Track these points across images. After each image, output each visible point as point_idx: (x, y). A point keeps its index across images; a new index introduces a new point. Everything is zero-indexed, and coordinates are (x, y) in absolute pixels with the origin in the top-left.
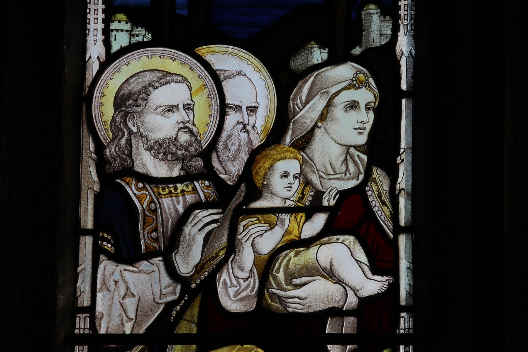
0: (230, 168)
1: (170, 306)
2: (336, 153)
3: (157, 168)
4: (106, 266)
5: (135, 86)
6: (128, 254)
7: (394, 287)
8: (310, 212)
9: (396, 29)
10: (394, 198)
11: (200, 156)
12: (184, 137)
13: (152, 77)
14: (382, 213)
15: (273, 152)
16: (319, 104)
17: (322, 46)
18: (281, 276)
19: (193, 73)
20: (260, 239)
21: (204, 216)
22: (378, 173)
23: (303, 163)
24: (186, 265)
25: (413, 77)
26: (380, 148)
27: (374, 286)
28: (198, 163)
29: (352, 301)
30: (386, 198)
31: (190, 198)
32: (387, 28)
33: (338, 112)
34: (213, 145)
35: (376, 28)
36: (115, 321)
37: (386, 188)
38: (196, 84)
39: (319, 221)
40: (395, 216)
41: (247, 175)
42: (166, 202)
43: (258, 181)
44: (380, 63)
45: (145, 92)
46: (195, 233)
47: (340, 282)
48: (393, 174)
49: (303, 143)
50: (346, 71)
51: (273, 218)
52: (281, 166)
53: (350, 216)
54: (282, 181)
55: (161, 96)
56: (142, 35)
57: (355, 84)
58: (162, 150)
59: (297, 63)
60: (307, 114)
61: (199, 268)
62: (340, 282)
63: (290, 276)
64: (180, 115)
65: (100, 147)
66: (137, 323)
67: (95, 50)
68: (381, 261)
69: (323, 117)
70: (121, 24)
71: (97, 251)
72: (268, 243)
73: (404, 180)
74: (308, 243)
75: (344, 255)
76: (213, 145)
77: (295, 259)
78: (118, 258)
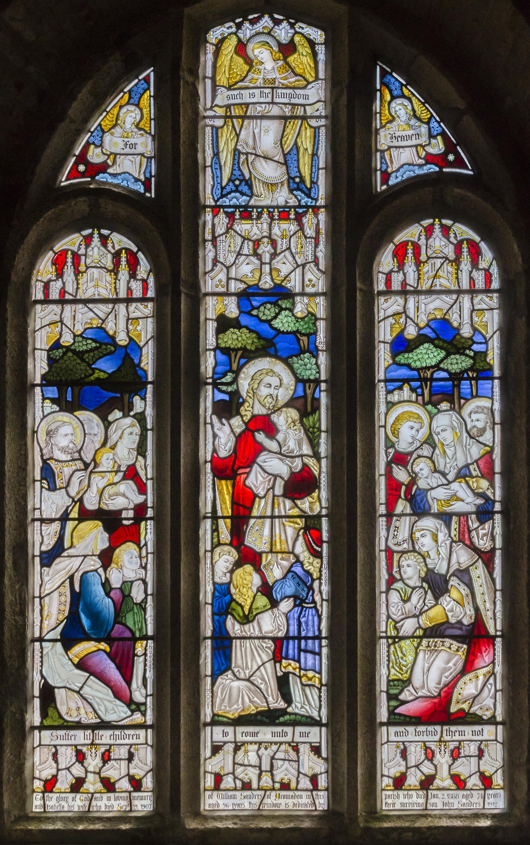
0: (88, 457)
1: (68, 507)
2: (126, 452)
3: (63, 457)
4: (45, 492)
5: (53, 427)
6: (52, 488)
7: (146, 500)
8: (117, 472)
9: (146, 405)
10: (147, 469)
11: (246, 52)
12: (71, 445)
13: (59, 423)
14: (142, 473)
15: (103, 450)
16: (119, 432)
17: (120, 410)
18: (107, 496)
19: (75, 422)
20: (98, 482)
21: (78, 474)
22: (140, 458)
23: (114, 454)
24: (73, 490)
25: (158, 358)
26: (141, 450)
27: (140, 499)
28: (76, 455)
29: (132, 506)
30: (143, 467)
31: (74, 468)
32: (143, 405)
33: (126, 435)
34: (81, 448)
35: (138, 404)
36: (49, 513)
37: (143, 464)
38: (75, 425)
39: (121, 475)
40: (146, 474)
41: (94, 460)
42: (65, 469)
43: (98, 462)
44: (141, 418)
45: (57, 429)
46: (75, 480)
47: (127, 498)
48: (145, 457)
49: (113, 448)
50: (128, 421)
51: (103, 474)
52: (105, 457)
53: (131, 474)
54: (106, 461)
55: (63, 430)
56: (56, 408)
57: (132, 426)
58: (63, 450)
59: (111, 418)
60: (114, 438)
61: (78, 493)
62: (127, 498)
63: (110, 496)
64: (70, 437)
65: (41, 450)
66: (56, 514)
67: (39, 414)
68: (142, 489)
69: (120, 438)
70: (48, 403)
71: (42, 487)
72: (101, 485)
73: (149, 461)
74: (116, 484)
75: (128, 488)
76: (81, 448)
77: (111, 490)
78: (49, 489)
